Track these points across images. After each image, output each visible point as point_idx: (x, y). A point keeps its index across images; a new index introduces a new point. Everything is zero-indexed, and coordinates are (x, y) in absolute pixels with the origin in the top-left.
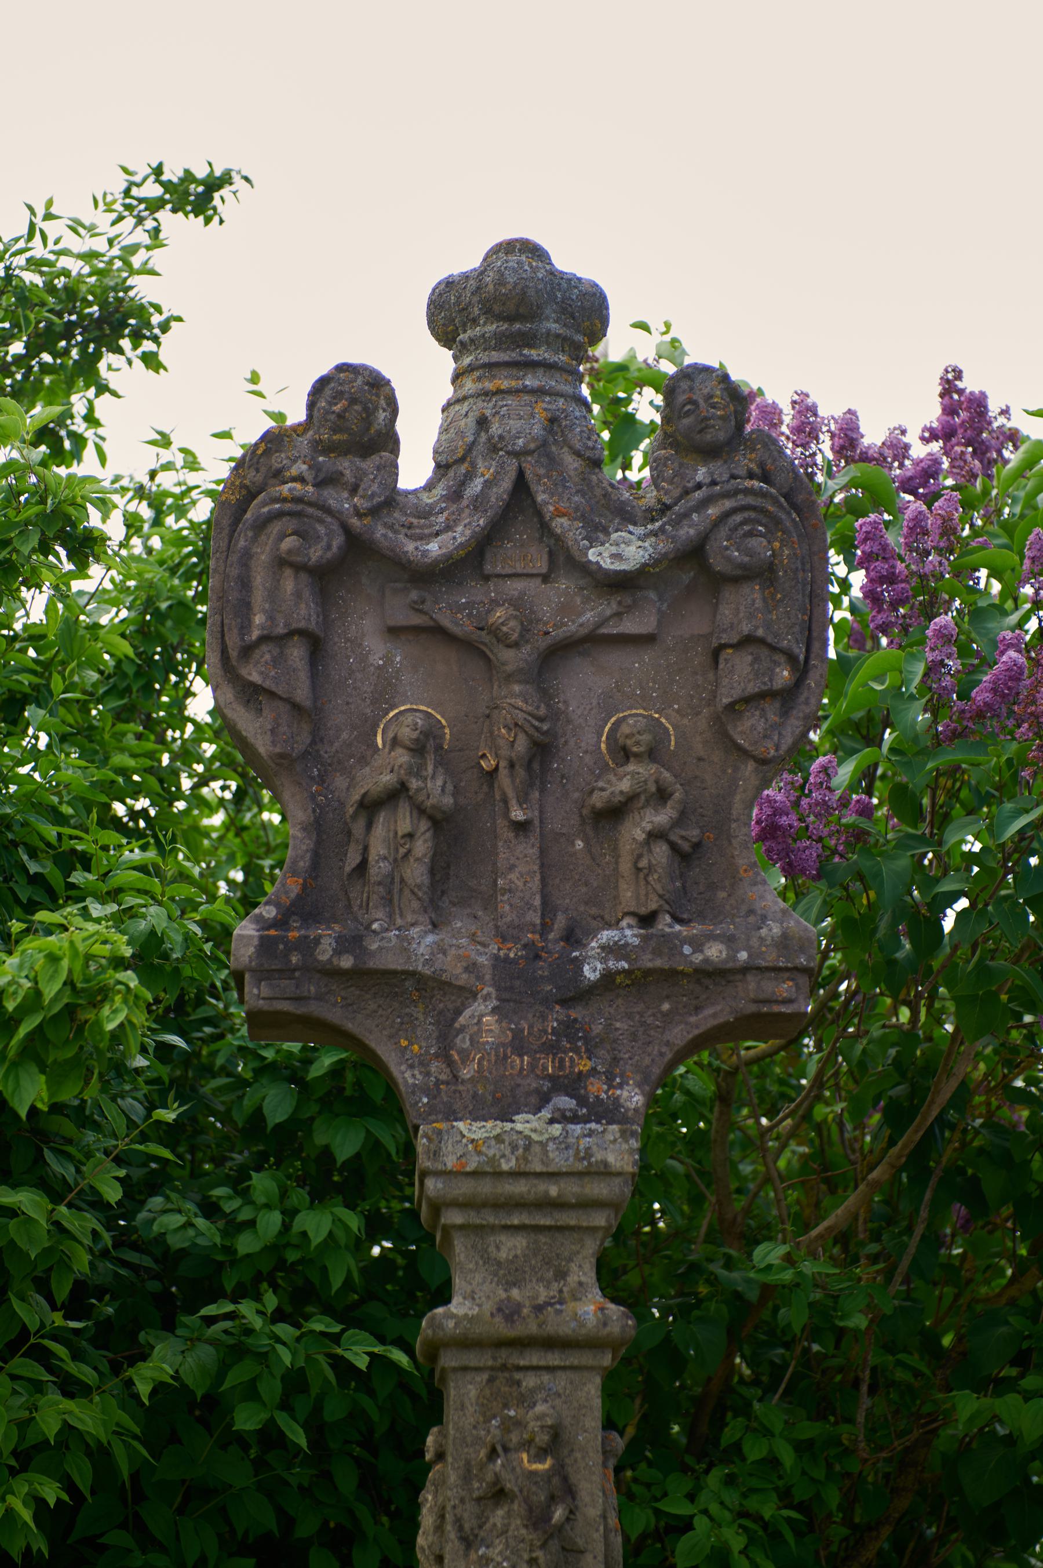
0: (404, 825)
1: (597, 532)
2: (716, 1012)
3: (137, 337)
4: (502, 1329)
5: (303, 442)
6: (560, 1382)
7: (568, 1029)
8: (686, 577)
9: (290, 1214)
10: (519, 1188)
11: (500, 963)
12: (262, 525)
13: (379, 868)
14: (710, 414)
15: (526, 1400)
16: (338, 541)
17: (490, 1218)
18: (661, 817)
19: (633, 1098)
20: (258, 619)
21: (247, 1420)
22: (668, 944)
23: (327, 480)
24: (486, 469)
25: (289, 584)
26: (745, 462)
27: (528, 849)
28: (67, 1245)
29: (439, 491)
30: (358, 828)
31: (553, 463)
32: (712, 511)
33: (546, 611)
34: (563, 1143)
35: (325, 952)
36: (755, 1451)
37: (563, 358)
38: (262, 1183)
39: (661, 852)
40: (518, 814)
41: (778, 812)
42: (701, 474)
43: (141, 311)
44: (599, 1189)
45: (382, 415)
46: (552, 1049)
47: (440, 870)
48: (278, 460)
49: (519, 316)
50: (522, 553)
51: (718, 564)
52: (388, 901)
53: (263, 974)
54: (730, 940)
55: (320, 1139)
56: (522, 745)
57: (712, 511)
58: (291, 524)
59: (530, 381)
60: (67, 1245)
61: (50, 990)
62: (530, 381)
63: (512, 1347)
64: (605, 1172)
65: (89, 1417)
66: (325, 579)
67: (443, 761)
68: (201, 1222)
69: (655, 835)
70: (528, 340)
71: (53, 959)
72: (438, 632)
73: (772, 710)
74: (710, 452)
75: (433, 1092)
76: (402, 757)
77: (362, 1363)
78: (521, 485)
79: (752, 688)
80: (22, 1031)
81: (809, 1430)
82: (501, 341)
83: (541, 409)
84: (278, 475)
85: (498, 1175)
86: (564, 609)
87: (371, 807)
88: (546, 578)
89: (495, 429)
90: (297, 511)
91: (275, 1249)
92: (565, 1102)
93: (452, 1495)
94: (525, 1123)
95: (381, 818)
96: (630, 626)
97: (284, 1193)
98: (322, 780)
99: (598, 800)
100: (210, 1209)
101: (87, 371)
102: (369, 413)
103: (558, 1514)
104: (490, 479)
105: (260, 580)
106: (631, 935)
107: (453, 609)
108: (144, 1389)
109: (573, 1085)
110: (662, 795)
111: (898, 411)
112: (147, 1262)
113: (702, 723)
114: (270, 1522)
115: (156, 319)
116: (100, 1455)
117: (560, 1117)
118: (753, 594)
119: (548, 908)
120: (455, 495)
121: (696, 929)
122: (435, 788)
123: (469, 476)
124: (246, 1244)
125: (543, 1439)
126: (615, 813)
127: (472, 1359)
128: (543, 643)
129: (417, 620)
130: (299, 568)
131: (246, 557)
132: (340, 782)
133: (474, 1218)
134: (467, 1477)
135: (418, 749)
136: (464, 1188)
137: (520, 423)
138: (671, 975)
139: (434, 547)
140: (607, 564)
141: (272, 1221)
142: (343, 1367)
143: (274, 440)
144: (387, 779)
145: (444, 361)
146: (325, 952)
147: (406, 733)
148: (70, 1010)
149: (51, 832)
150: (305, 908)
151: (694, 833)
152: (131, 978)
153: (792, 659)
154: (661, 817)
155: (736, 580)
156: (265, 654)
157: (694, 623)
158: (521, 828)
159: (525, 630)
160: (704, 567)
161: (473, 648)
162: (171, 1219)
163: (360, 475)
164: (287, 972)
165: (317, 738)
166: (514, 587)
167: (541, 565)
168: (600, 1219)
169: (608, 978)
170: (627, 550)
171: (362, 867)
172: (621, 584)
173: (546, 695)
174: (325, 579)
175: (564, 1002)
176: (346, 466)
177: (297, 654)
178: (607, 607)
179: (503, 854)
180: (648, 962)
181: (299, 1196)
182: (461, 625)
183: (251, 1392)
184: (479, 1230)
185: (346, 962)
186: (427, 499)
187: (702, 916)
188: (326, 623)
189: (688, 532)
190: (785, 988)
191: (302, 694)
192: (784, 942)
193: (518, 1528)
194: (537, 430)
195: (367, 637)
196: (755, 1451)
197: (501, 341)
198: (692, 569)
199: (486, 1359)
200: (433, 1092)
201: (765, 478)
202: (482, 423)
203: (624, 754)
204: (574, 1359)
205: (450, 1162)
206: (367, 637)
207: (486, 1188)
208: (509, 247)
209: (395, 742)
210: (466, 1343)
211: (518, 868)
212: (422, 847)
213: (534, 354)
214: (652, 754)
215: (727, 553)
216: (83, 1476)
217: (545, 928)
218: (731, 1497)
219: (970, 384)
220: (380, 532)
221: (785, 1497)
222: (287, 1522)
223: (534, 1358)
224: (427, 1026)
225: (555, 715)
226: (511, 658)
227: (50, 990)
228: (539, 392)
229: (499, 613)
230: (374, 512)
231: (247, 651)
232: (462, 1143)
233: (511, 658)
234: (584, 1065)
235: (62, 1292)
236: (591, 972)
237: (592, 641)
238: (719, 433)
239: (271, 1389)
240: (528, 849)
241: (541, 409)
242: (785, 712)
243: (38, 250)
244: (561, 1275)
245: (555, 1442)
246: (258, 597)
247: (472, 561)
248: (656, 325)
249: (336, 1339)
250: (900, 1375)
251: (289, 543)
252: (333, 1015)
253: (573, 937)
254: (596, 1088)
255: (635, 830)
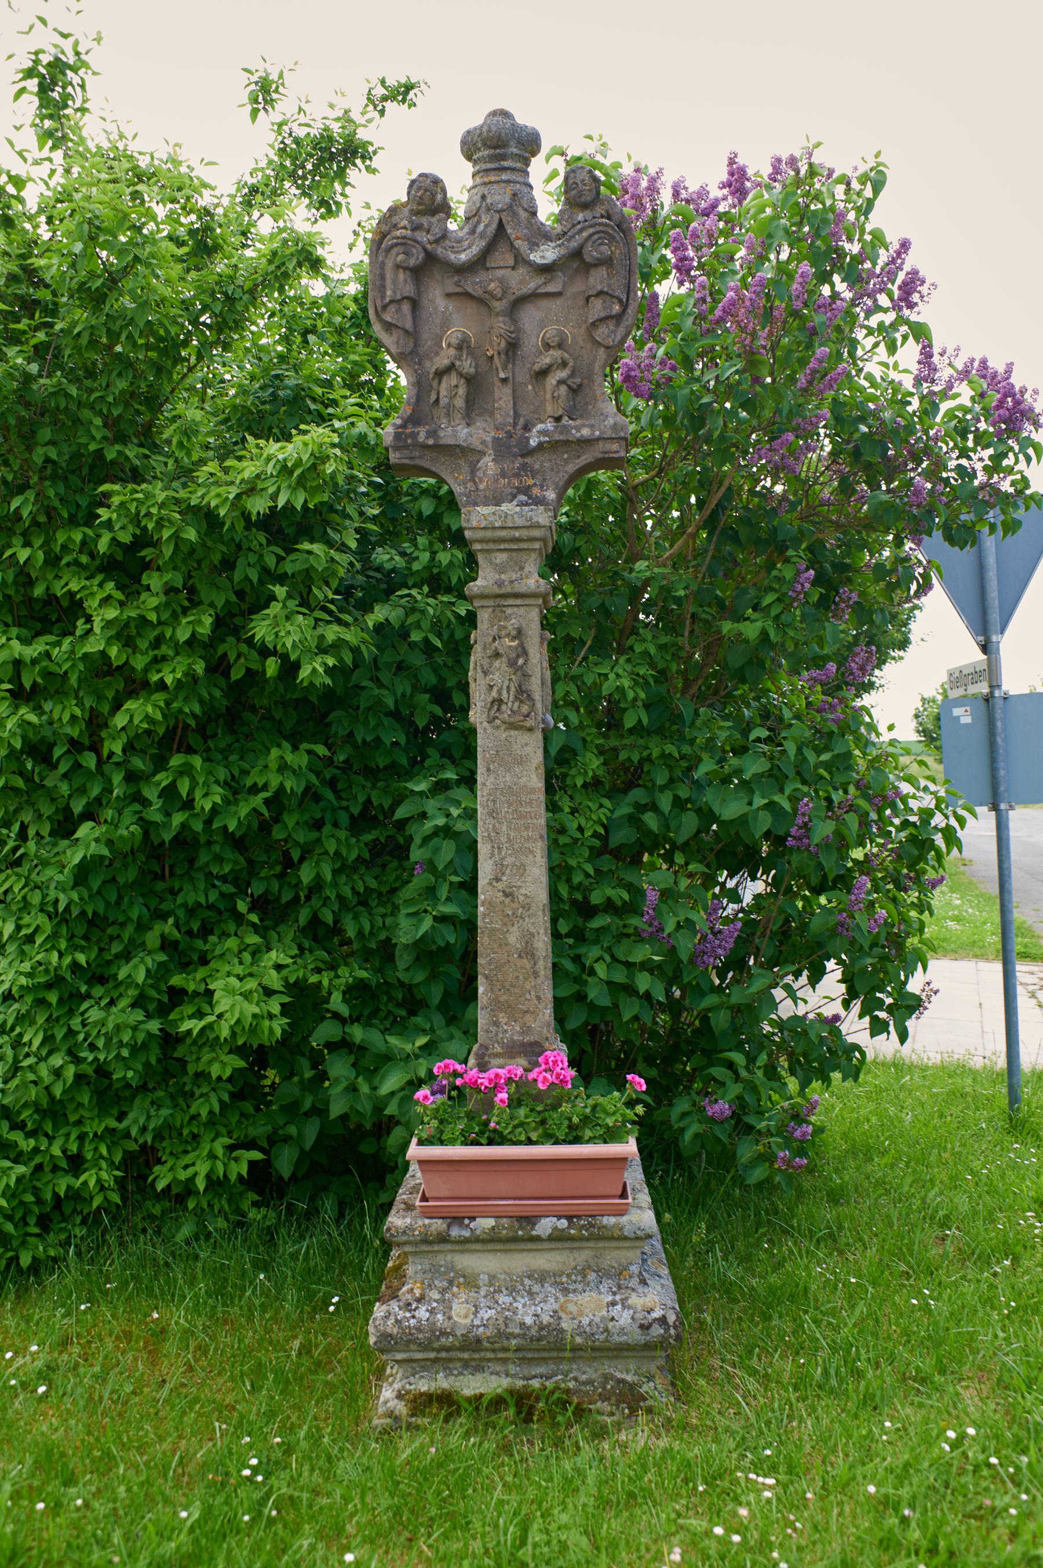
0: (454, 382)
1: (534, 246)
2: (586, 458)
3: (363, 157)
4: (497, 590)
5: (406, 211)
6: (522, 610)
7: (524, 467)
8: (575, 265)
9: (434, 553)
10: (503, 534)
11: (495, 440)
12: (389, 250)
13: (444, 401)
14: (584, 188)
15: (507, 618)
16: (422, 256)
17: (492, 546)
18: (563, 374)
19: (551, 495)
20: (389, 293)
21: (416, 636)
22: (566, 429)
23: (416, 228)
24: (485, 219)
25: (401, 276)
26: (600, 210)
27: (507, 390)
28: (335, 566)
29: (466, 230)
30: (435, 384)
31: (515, 214)
32: (585, 234)
33: (513, 283)
34: (521, 515)
35: (422, 438)
36: (639, 648)
37: (519, 165)
38: (422, 541)
39: (563, 389)
40: (502, 375)
41: (630, 369)
42: (580, 217)
43: (366, 144)
44: (536, 533)
45: (439, 197)
46: (517, 475)
47: (470, 402)
48: (395, 219)
49: (502, 147)
50: (503, 258)
51: (588, 259)
52: (448, 415)
53: (396, 448)
54: (592, 427)
55: (446, 521)
56: (503, 344)
57: (585, 234)
58: (400, 249)
59: (504, 177)
60: (335, 566)
61: (305, 458)
62: (504, 177)
63: (501, 598)
64: (538, 526)
65: (350, 636)
66: (418, 273)
67: (471, 352)
68: (397, 558)
69: (560, 382)
70: (503, 157)
71: (306, 444)
72: (467, 295)
73: (612, 324)
74: (585, 206)
75: (468, 496)
76: (452, 352)
77: (463, 613)
78: (501, 226)
79: (603, 315)
80: (296, 474)
81: (665, 639)
82: (492, 158)
83: (509, 189)
84: (395, 226)
85: (494, 528)
86: (522, 282)
87: (440, 374)
88: (513, 268)
89: (489, 200)
90: (404, 243)
91: (427, 568)
92: (523, 498)
93: (479, 655)
94: (505, 507)
95: (445, 379)
96: (550, 289)
97: (431, 544)
98: (420, 363)
99: (536, 367)
100: (403, 554)
101: (341, 174)
102: (433, 196)
103: (521, 661)
104: (487, 224)
105: (389, 275)
106: (550, 425)
107: (473, 284)
108: (371, 624)
109: (526, 490)
110: (564, 364)
111: (708, 178)
112: (378, 576)
113: (582, 331)
114: (434, 680)
115: (371, 149)
116: (356, 651)
117: (521, 504)
118: (603, 271)
119: (516, 416)
120: (473, 232)
121: (579, 422)
122: (467, 365)
123: (478, 222)
124: (416, 566)
125: (514, 633)
126: (543, 373)
127: (485, 603)
128: (512, 298)
129: (458, 290)
130: (405, 269)
131: (383, 265)
132: (427, 364)
133: (485, 546)
134: (484, 649)
135: (459, 348)
136: (480, 534)
137: (500, 197)
138: (567, 443)
139: (463, 257)
140: (539, 261)
141: (426, 556)
142: (458, 616)
143: (393, 210)
144: (446, 362)
145: (469, 168)
146: (422, 438)
147: (454, 341)
148: (314, 466)
149: (319, 391)
150: (414, 419)
151: (578, 380)
152: (338, 451)
153: (620, 301)
154: (563, 374)
155: (596, 266)
156: (392, 308)
157: (578, 286)
158: (504, 381)
159: (504, 292)
160: (583, 260)
161: (482, 301)
162: (382, 556)
163: (431, 224)
164: (406, 447)
165: (416, 344)
166: (500, 273)
167: (511, 263)
168: (537, 545)
169: (541, 445)
170: (547, 254)
171: (437, 401)
172: (546, 270)
173: (514, 321)
174: (418, 273)
175: (523, 456)
176: (424, 220)
177: (406, 307)
178: (540, 280)
179: (497, 393)
180: (557, 437)
181: (438, 546)
182: (477, 291)
183: (418, 625)
184: (488, 551)
185: (431, 442)
186: (460, 234)
187: (582, 416)
188: (419, 292)
189: (574, 244)
190: (615, 447)
191: (409, 326)
192: (615, 427)
193: (505, 667)
194: (507, 200)
195: (437, 298)
196: (639, 648)
197: (492, 158)
198: (576, 261)
199: (491, 603)
200: (468, 496)
201: (609, 218)
202: (483, 197)
203: (548, 346)
204: (527, 602)
205: (474, 524)
206: (437, 298)
207: (489, 534)
208: (494, 113)
209: (449, 345)
210: (483, 596)
211: (503, 398)
212: (462, 391)
213: (505, 164)
214: (560, 346)
215: (591, 253)
216: (348, 658)
217: (515, 424)
218: (629, 667)
219: (740, 160)
220: (439, 251)
221: (652, 665)
222: (442, 679)
223: (511, 602)
224: (465, 468)
225: (518, 330)
226: (498, 306)
227: (305, 458)
228: (508, 182)
229: (493, 285)
230: (437, 241)
231: (385, 307)
232: (477, 517)
233: (498, 306)
234: (531, 482)
235: (334, 584)
236: (533, 443)
237: (533, 297)
238: (588, 198)
239: (426, 624)
240: (507, 390)
241: (509, 189)
242: (617, 325)
243: (303, 119)
244: (522, 568)
245: (519, 634)
246: (389, 284)
247: (480, 262)
248: (595, 136)
249: (453, 604)
250: (704, 616)
251: (401, 257)
252: (427, 464)
253: (527, 428)
254: (536, 491)
255: (552, 380)
